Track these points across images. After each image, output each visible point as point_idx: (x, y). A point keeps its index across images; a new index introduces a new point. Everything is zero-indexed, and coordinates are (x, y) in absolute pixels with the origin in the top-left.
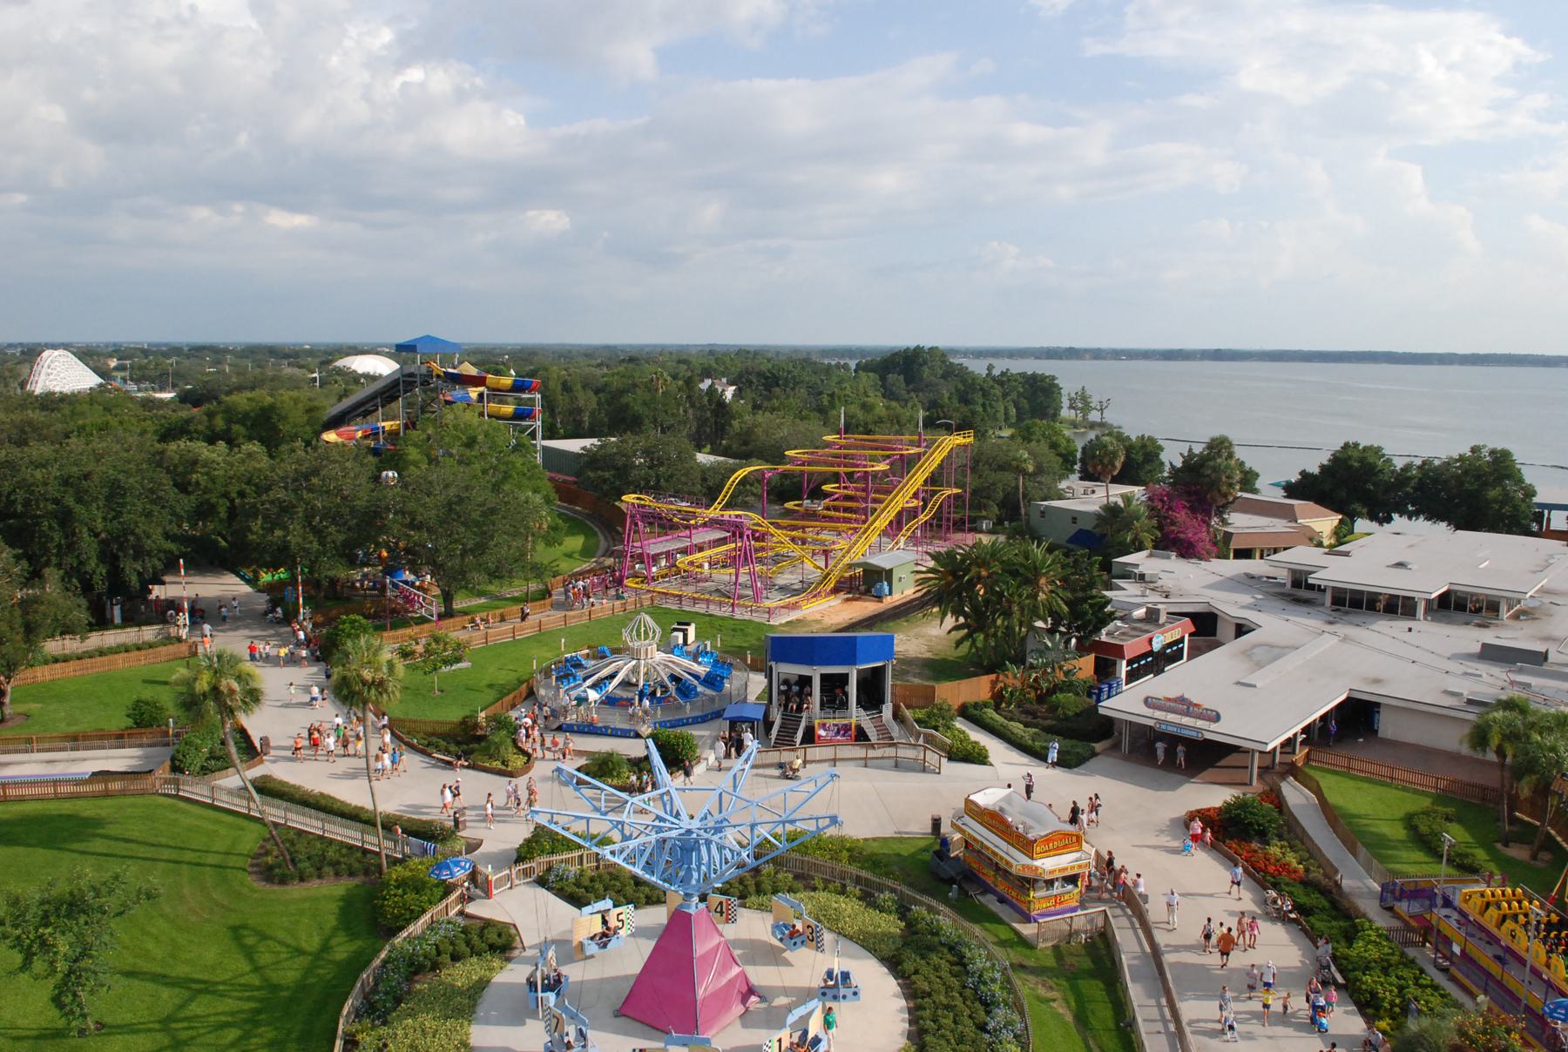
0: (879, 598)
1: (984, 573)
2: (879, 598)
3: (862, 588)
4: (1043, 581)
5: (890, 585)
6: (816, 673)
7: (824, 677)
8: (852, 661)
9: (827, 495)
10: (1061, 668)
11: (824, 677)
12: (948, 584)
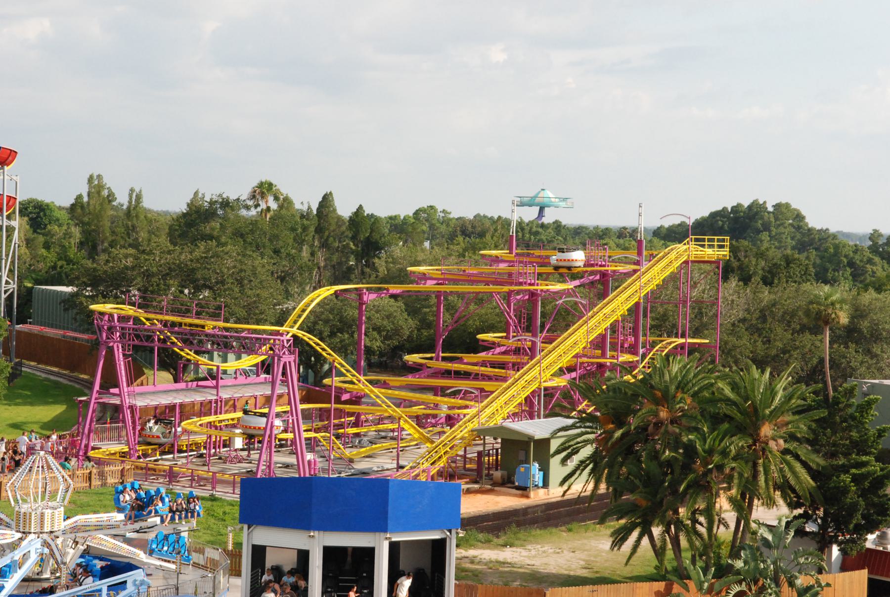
0: (524, 490)
1: (663, 414)
2: (524, 490)
3: (498, 474)
4: (766, 430)
5: (545, 469)
6: (316, 543)
7: (329, 553)
8: (379, 525)
9: (488, 346)
10: (791, 584)
11: (329, 553)
12: (609, 434)
